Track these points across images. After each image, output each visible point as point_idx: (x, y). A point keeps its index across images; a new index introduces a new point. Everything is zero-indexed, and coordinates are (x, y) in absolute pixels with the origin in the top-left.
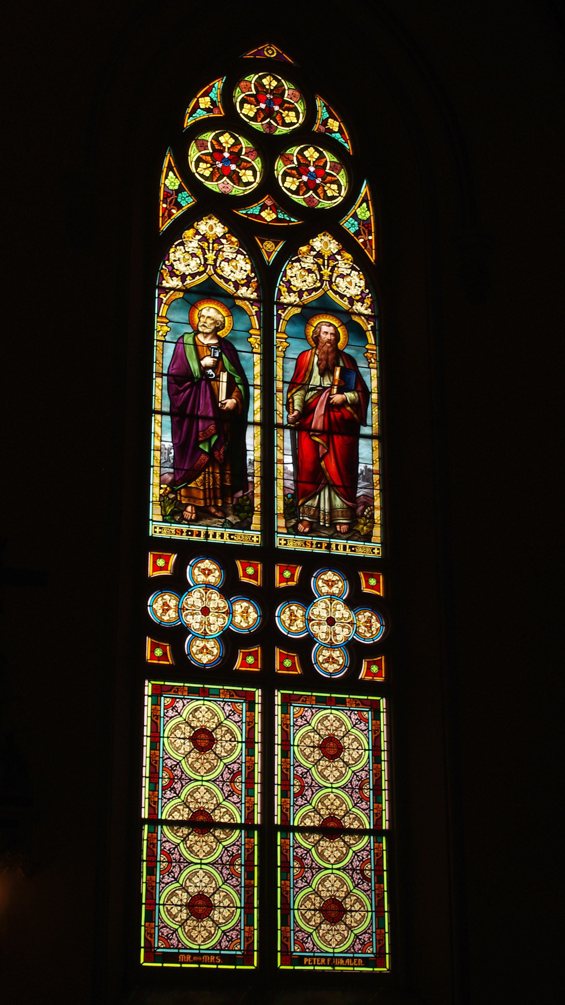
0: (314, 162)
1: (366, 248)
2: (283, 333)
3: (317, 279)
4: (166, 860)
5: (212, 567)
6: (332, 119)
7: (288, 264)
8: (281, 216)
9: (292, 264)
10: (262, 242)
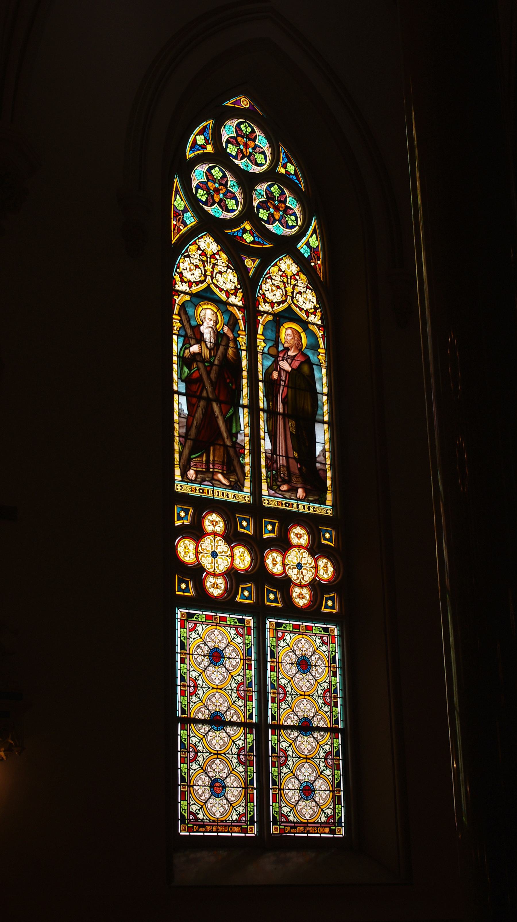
3: (202, 273)
6: (290, 163)
7: (181, 258)
9: (184, 258)
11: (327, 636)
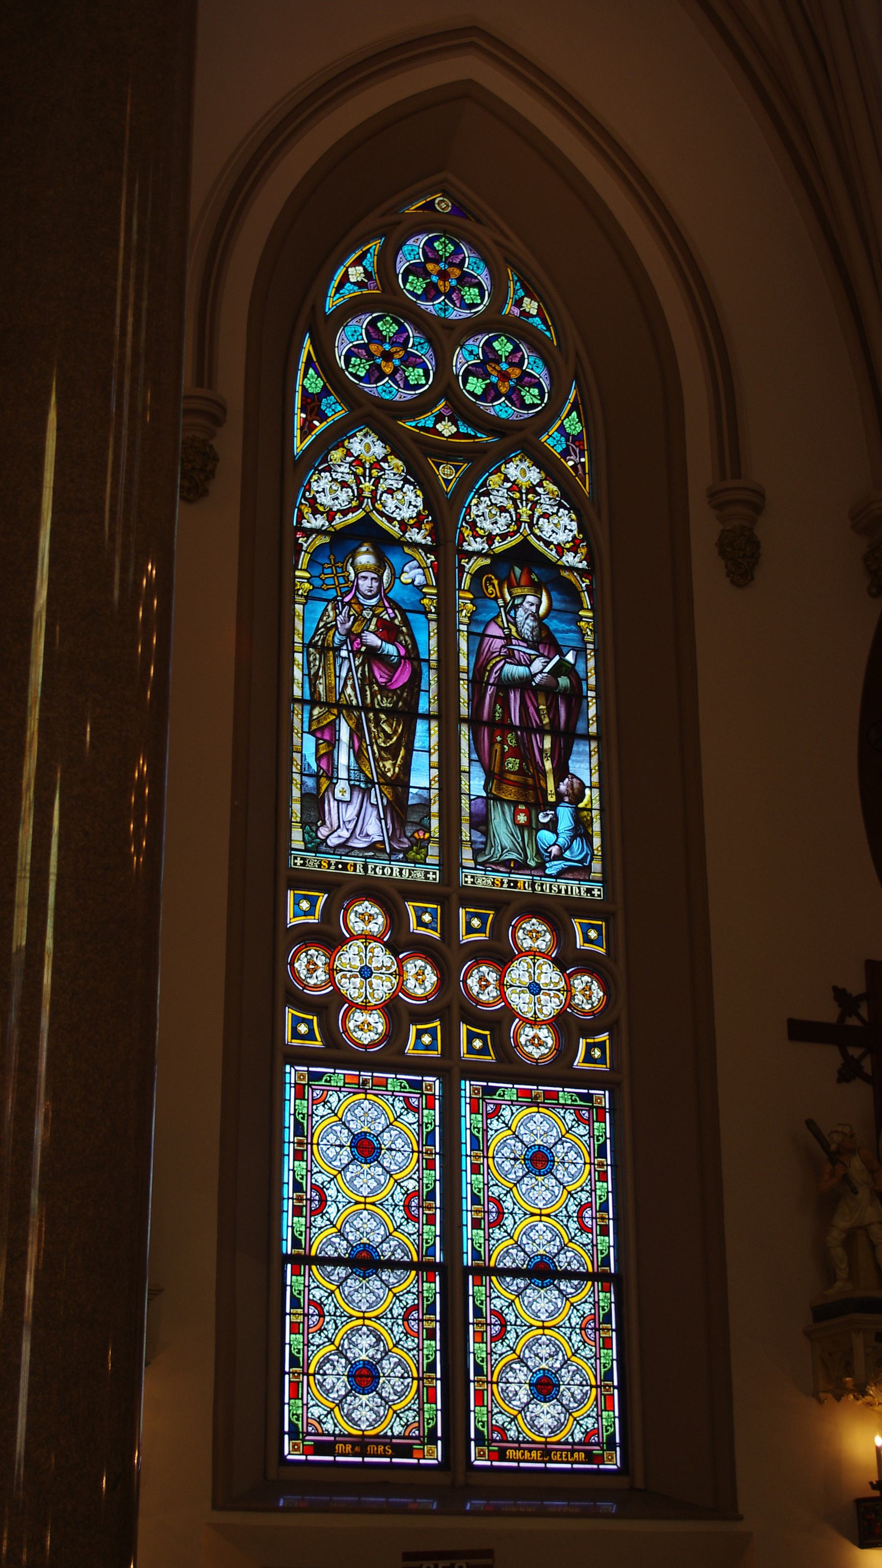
0: (506, 357)
1: (577, 475)
2: (466, 591)
3: (354, 495)
4: (499, 1322)
5: (375, 910)
7: (473, 498)
8: (463, 429)
9: (479, 498)
10: (438, 465)
11: (484, 1103)
